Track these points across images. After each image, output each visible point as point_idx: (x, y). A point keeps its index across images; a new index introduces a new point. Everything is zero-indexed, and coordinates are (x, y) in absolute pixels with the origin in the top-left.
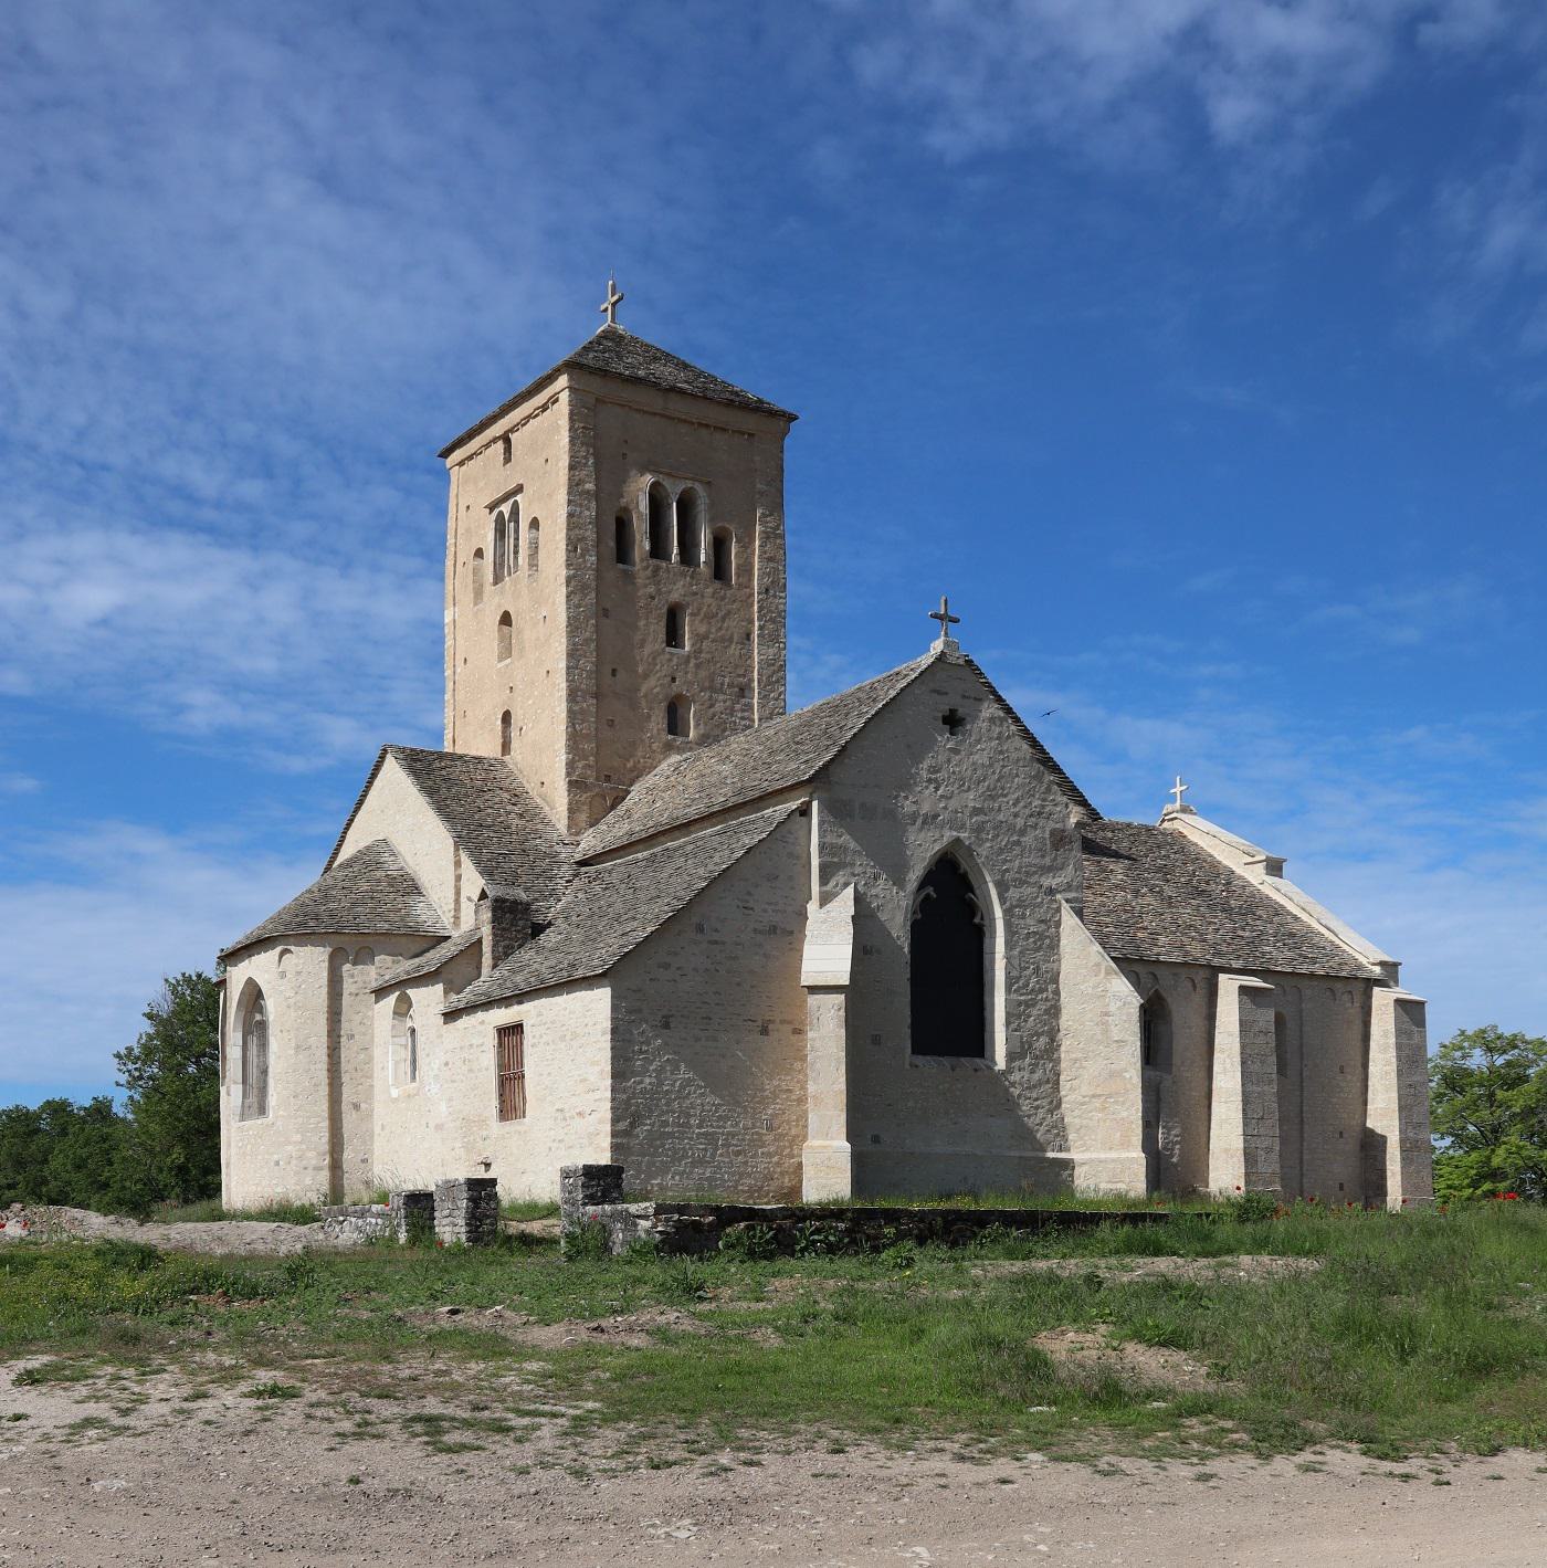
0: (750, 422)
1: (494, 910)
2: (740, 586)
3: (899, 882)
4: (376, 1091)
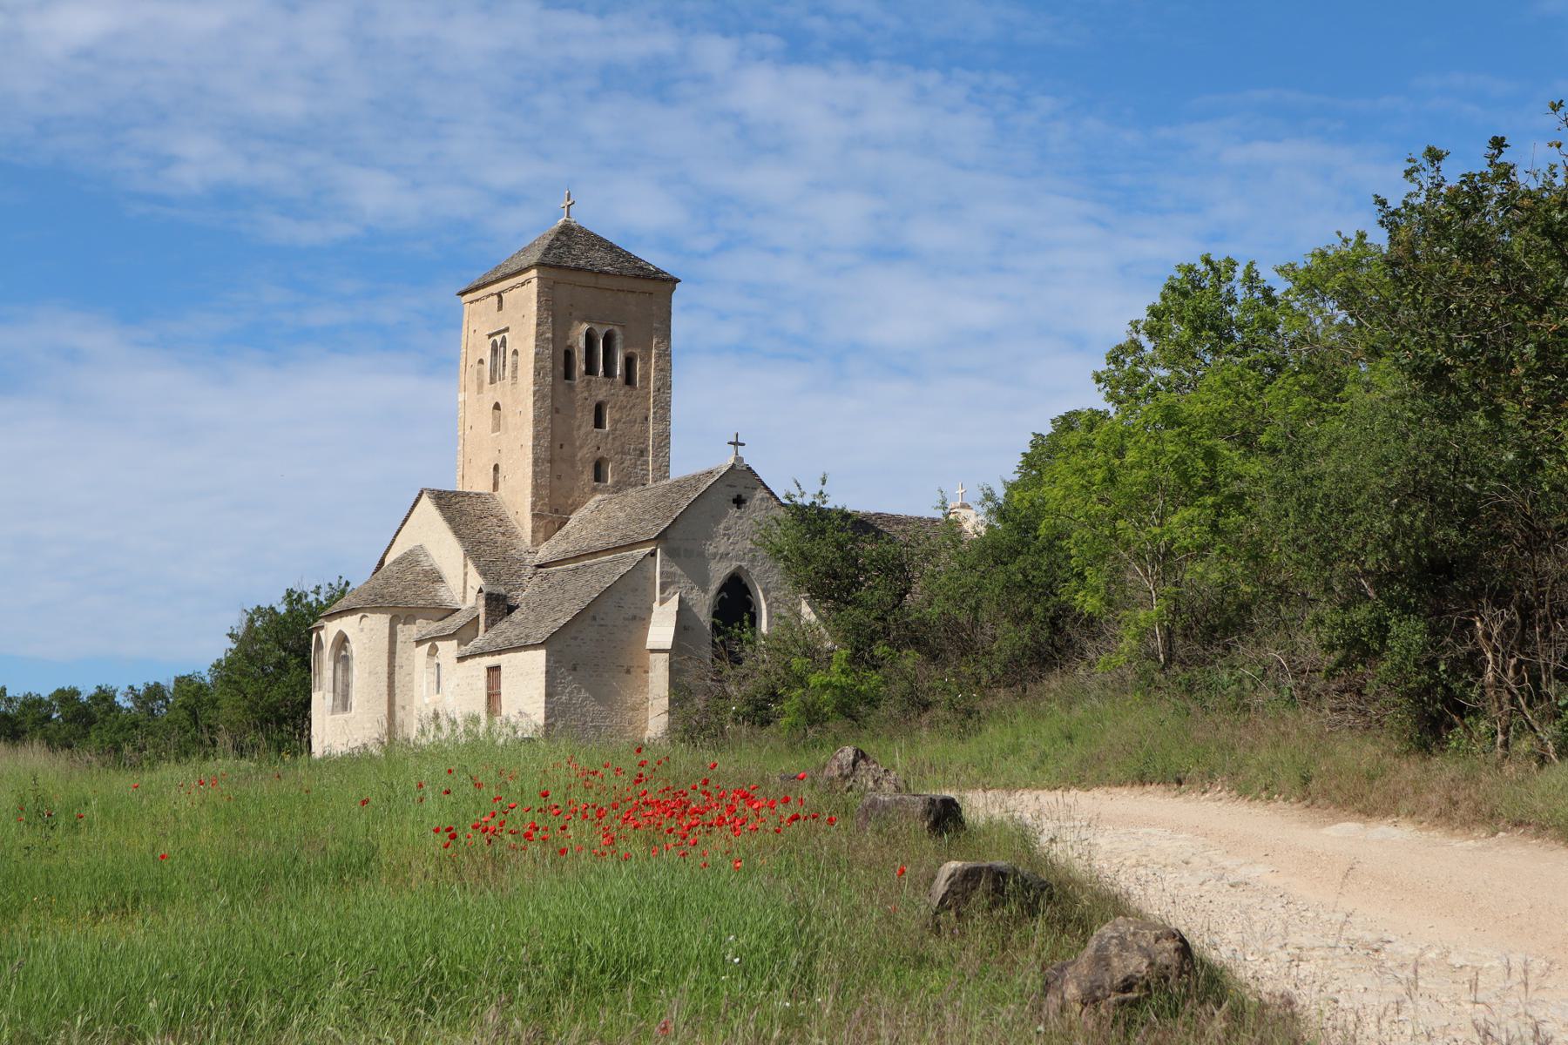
0: (650, 286)
1: (487, 600)
2: (642, 387)
3: (705, 591)
4: (416, 699)
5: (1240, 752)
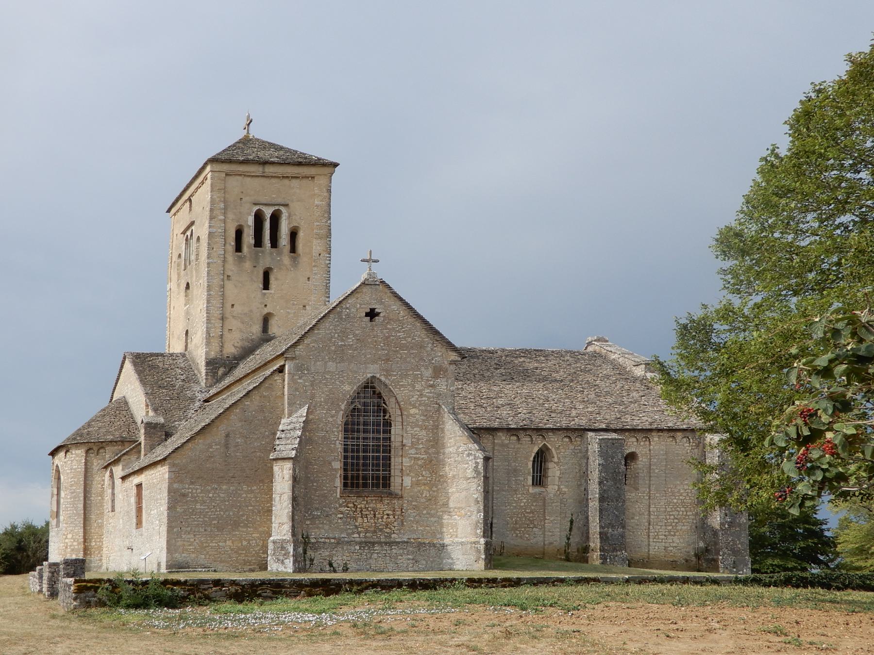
0: (312, 171)
5: (65, 604)
